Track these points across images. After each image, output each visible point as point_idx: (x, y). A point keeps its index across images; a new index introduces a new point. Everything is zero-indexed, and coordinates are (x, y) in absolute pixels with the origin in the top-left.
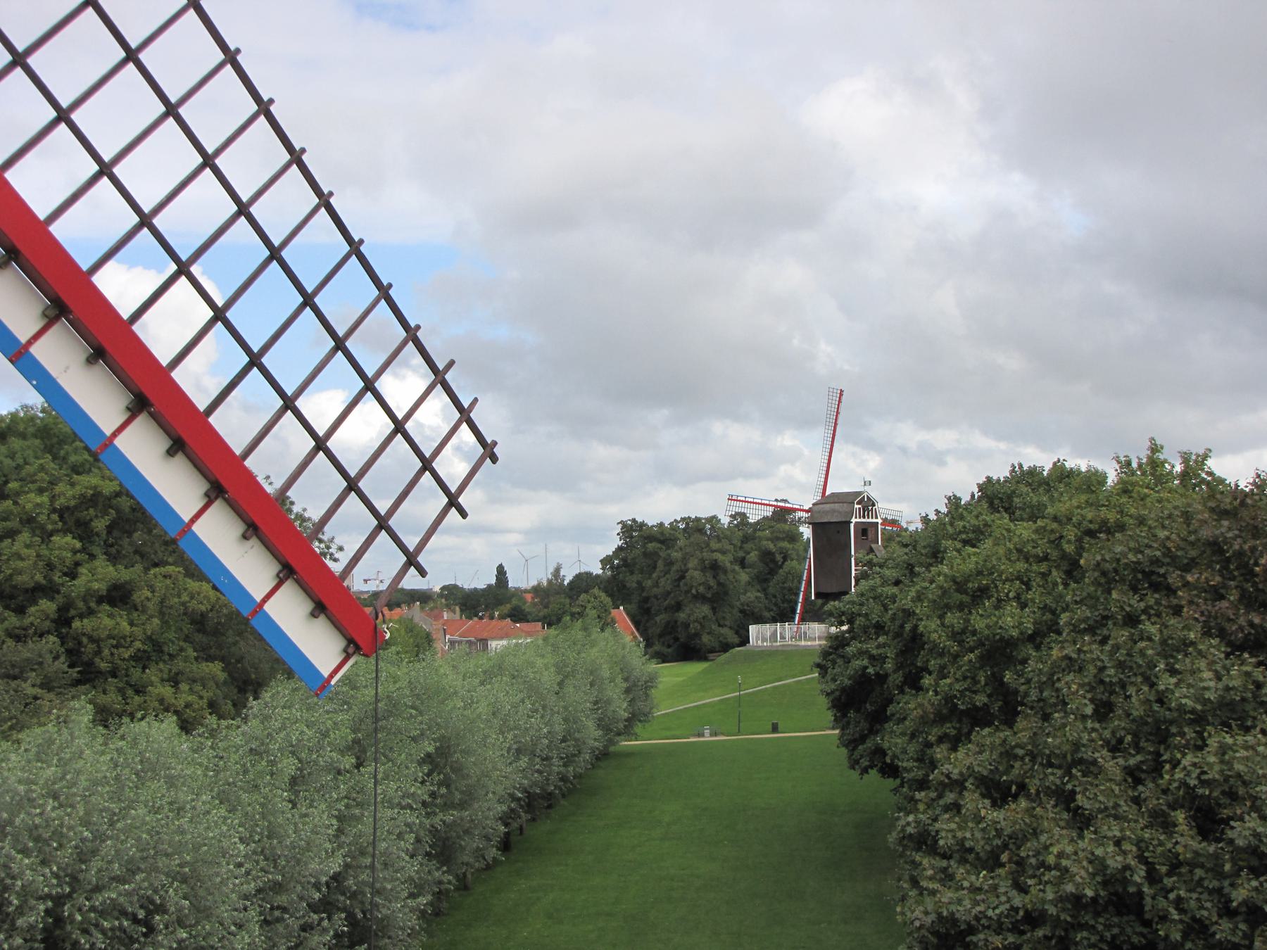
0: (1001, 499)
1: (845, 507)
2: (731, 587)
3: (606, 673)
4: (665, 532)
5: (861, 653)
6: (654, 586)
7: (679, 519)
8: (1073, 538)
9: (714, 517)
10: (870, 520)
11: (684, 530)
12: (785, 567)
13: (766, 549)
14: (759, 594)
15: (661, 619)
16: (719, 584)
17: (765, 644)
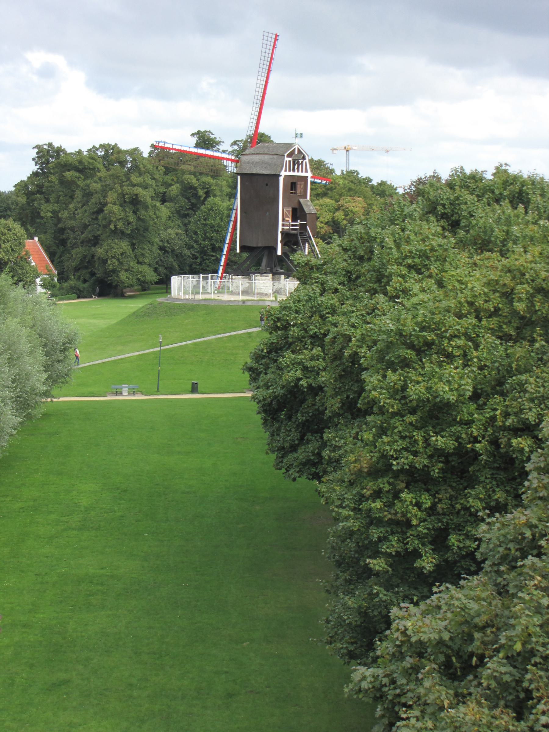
0: (444, 205)
1: (275, 160)
2: (152, 223)
3: (24, 346)
4: (84, 161)
5: (295, 363)
6: (70, 218)
7: (98, 146)
8: (523, 296)
9: (136, 150)
10: (300, 174)
11: (104, 157)
12: (206, 203)
13: (189, 183)
14: (180, 231)
15: (78, 252)
16: (139, 219)
17: (187, 297)
